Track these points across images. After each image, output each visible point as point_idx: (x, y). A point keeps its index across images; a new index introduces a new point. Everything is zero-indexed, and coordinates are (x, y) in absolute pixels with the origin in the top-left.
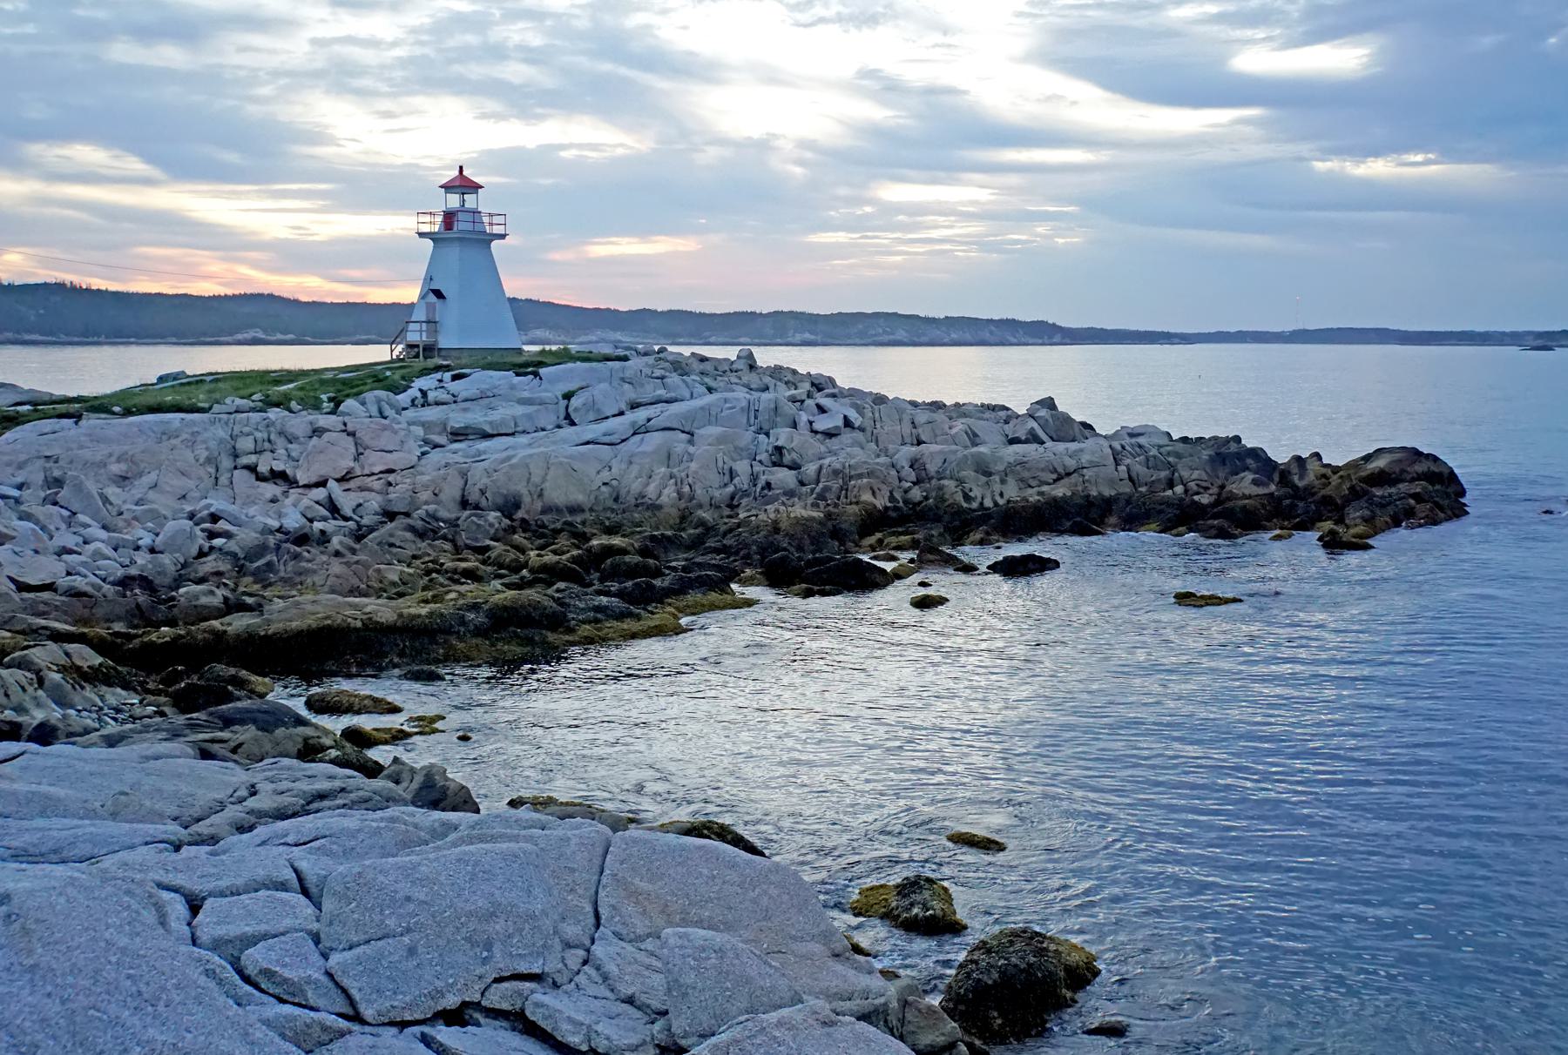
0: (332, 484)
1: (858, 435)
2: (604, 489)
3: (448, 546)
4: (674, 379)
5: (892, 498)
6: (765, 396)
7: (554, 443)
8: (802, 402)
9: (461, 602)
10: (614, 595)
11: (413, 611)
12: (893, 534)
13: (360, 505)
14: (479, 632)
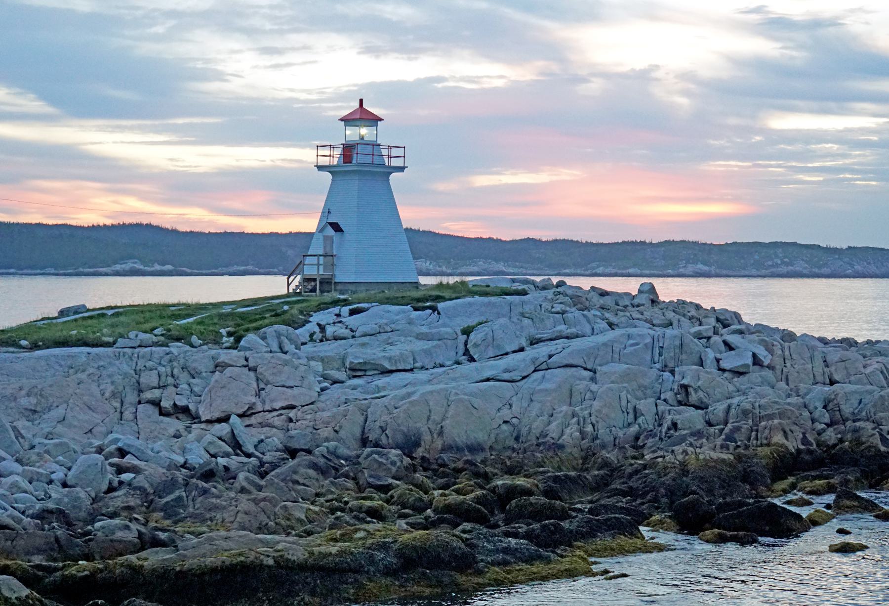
0: (234, 419)
1: (768, 373)
2: (504, 427)
3: (350, 484)
4: (574, 314)
5: (805, 441)
6: (669, 332)
7: (454, 379)
8: (709, 338)
9: (370, 541)
10: (523, 538)
11: (323, 549)
12: (805, 478)
13: (262, 441)
14: (390, 572)
